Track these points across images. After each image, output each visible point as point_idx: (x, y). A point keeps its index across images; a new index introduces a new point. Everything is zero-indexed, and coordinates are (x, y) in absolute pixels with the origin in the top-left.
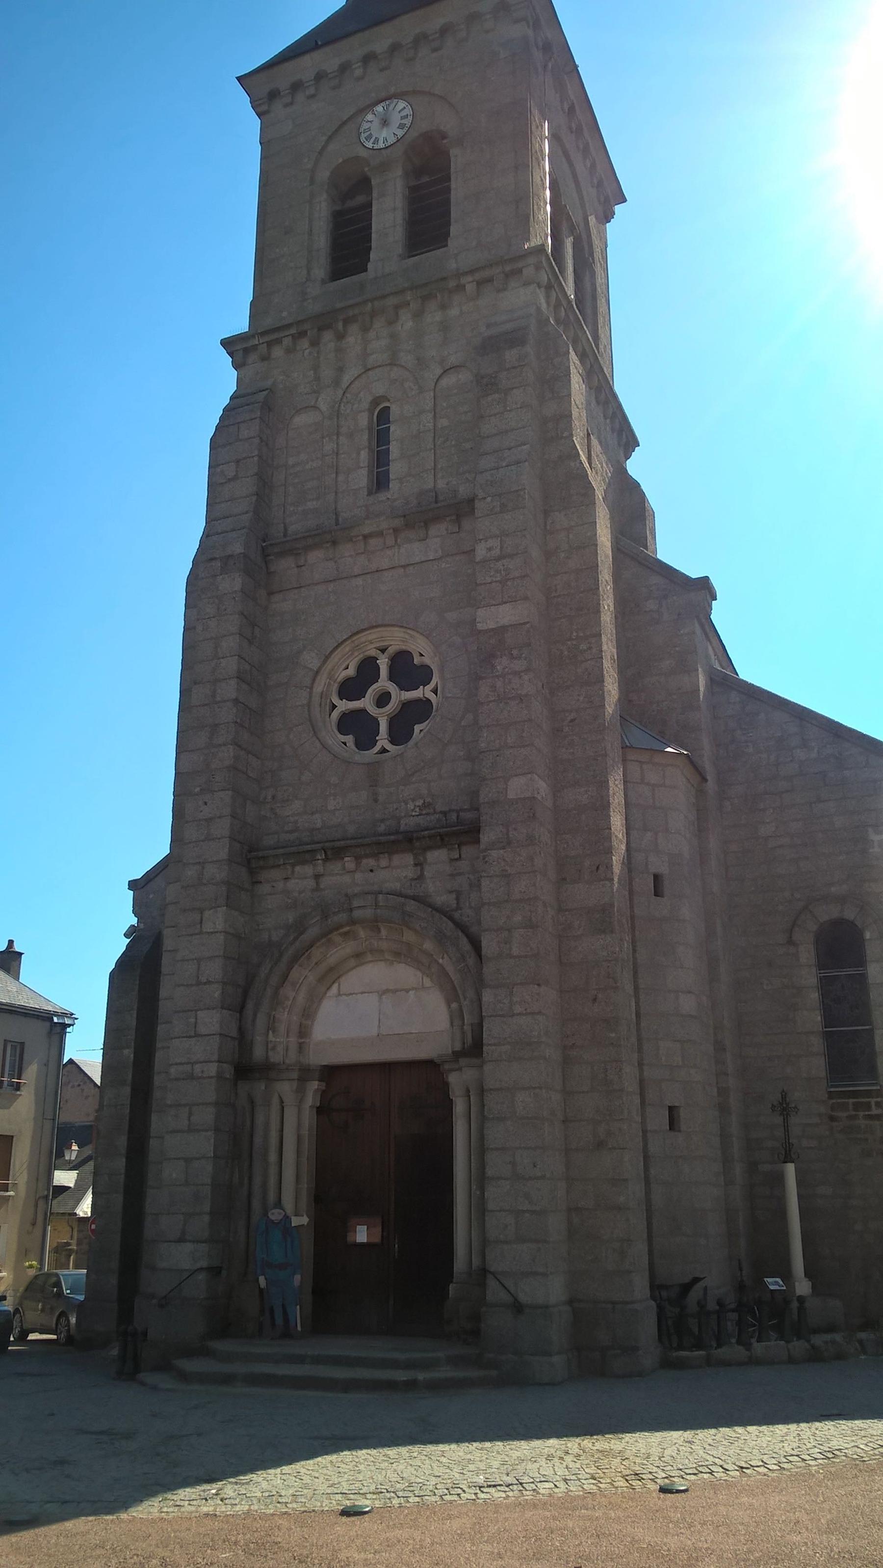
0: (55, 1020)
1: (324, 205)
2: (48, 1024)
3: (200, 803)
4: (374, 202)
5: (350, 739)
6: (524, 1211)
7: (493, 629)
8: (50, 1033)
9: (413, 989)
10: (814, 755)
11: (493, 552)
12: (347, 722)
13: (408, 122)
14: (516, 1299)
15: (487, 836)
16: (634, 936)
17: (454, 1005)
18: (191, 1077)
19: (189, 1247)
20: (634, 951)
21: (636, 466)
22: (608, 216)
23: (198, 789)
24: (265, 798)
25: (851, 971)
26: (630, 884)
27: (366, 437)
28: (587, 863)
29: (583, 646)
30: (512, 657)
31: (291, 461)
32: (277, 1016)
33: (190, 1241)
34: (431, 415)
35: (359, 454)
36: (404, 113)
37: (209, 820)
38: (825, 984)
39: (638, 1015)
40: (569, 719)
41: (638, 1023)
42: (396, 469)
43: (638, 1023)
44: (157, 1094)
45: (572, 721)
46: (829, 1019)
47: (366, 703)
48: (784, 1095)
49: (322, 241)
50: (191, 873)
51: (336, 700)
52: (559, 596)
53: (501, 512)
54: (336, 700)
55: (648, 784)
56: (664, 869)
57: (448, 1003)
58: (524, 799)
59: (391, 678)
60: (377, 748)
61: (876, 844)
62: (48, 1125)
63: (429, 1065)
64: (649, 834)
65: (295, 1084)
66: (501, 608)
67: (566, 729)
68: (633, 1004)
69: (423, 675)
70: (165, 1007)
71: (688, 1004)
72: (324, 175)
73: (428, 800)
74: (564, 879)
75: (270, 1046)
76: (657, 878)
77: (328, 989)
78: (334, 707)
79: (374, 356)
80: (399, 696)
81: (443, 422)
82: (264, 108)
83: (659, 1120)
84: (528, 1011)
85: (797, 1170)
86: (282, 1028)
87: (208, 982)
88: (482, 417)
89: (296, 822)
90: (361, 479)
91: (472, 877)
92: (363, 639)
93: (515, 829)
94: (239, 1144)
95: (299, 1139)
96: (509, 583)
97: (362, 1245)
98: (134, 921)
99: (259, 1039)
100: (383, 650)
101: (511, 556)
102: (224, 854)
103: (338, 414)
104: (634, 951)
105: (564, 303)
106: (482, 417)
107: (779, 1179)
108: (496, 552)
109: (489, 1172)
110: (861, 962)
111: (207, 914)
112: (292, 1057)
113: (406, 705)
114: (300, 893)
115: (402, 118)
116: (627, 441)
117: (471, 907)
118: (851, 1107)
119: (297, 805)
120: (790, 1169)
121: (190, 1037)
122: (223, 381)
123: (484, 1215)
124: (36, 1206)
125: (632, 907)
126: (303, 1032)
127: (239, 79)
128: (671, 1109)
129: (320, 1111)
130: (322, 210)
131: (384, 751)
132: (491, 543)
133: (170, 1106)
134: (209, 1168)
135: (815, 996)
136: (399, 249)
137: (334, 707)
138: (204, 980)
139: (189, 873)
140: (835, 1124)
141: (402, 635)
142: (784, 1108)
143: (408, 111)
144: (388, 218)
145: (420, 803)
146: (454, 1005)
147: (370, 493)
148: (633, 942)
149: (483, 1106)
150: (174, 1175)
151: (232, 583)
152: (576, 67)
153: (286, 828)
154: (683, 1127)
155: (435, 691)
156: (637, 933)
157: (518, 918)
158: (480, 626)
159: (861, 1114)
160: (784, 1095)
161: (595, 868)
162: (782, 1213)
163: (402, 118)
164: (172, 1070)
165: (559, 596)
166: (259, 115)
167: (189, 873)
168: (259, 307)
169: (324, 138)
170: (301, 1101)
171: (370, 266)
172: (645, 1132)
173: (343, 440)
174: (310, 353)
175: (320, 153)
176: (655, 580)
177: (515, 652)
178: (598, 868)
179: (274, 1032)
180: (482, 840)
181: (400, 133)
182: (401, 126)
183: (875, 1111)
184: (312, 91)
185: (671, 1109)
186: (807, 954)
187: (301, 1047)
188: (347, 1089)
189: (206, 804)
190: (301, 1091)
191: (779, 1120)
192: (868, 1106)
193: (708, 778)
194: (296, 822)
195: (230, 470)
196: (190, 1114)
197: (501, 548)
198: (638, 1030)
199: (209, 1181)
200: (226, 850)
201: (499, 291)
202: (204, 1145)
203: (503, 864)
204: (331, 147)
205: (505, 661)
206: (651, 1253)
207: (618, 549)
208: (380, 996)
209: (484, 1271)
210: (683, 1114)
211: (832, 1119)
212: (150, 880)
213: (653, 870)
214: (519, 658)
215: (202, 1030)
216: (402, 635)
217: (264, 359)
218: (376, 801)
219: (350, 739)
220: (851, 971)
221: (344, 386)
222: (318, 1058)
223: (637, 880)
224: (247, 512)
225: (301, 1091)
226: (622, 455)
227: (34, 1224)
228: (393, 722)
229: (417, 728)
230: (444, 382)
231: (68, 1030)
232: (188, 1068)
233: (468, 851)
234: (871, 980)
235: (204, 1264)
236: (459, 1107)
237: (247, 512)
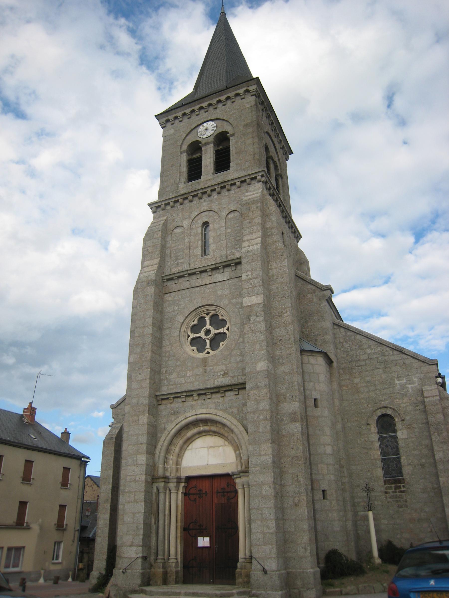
0: (83, 459)
1: (185, 157)
2: (79, 461)
3: (138, 374)
4: (203, 156)
5: (195, 348)
6: (267, 533)
7: (249, 306)
8: (81, 465)
9: (221, 446)
10: (373, 351)
11: (249, 277)
12: (194, 342)
13: (215, 129)
14: (264, 568)
15: (248, 386)
16: (307, 423)
17: (238, 452)
18: (135, 481)
19: (134, 548)
20: (308, 429)
21: (301, 245)
22: (287, 159)
23: (137, 368)
24: (163, 372)
25: (391, 434)
26: (305, 403)
27: (200, 236)
28: (288, 395)
29: (284, 311)
30: (257, 316)
31: (173, 245)
32: (168, 457)
33: (135, 546)
34: (224, 228)
35: (198, 242)
36: (213, 126)
37: (141, 380)
38: (381, 439)
39: (310, 454)
40: (280, 339)
41: (310, 458)
42: (212, 247)
43: (310, 458)
44: (121, 488)
45: (281, 340)
46: (384, 453)
47: (202, 334)
48: (367, 484)
49: (184, 169)
50: (135, 401)
51: (190, 333)
52: (274, 293)
53: (251, 262)
54: (190, 333)
55: (311, 364)
56: (318, 397)
57: (235, 451)
58: (263, 370)
59: (211, 325)
60: (206, 352)
61: (398, 384)
62: (80, 501)
63: (227, 476)
64: (312, 383)
65: (175, 484)
66: (253, 297)
67: (279, 343)
68: (308, 450)
69: (223, 323)
70: (124, 454)
71: (329, 450)
72: (185, 147)
73: (226, 372)
74: (279, 401)
75: (165, 469)
76: (315, 400)
77: (188, 446)
78: (189, 336)
79: (203, 208)
80: (214, 331)
81: (229, 231)
82: (164, 125)
83: (319, 495)
84: (267, 453)
85: (374, 514)
86: (170, 462)
87: (141, 444)
88: (243, 228)
89: (175, 381)
90: (199, 251)
91: (243, 401)
92: (200, 311)
93: (260, 382)
94: (153, 509)
95: (177, 506)
96: (255, 288)
97: (203, 535)
98: (112, 420)
99: (161, 466)
100: (207, 314)
101: (256, 278)
102: (147, 394)
103: (190, 228)
104: (308, 429)
105: (272, 188)
106: (243, 228)
107: (366, 518)
108: (250, 277)
109: (252, 518)
110: (395, 431)
111: (141, 417)
112: (173, 475)
113: (216, 335)
114: (177, 408)
115: (213, 127)
116: (298, 236)
117: (243, 413)
118: (393, 488)
119: (175, 375)
120: (370, 514)
121: (135, 465)
122: (147, 217)
123: (251, 535)
124: (74, 534)
125: (306, 412)
126: (178, 463)
127: (155, 116)
128: (324, 491)
129: (185, 494)
130: (184, 158)
131: (208, 353)
132: (248, 273)
133: (127, 492)
134: (142, 517)
135: (377, 445)
136: (212, 171)
137: (189, 336)
138: (139, 443)
139: (134, 401)
140: (387, 495)
141: (215, 308)
142: (368, 489)
143: (215, 125)
144: (208, 159)
145: (222, 373)
146: (238, 452)
147: (202, 256)
148: (307, 425)
149: (250, 491)
150: (129, 520)
151: (151, 290)
152: (273, 110)
153: (171, 383)
154: (328, 498)
155: (228, 329)
156: (309, 422)
157: (262, 417)
158: (244, 305)
159: (397, 490)
160: (367, 484)
161: (291, 397)
162: (369, 532)
163: (213, 127)
164: (128, 478)
165: (274, 293)
166: (162, 128)
167: (134, 401)
168: (161, 193)
169: (185, 135)
170: (178, 490)
171: (202, 177)
172: (313, 501)
173: (192, 237)
174: (180, 207)
175: (184, 140)
176: (310, 286)
177: (258, 314)
178: (292, 396)
179: (167, 463)
180: (247, 387)
181: (212, 132)
182: (212, 130)
183: (403, 489)
184: (181, 119)
185: (324, 491)
186: (374, 428)
187: (177, 470)
188: (196, 486)
189: (140, 374)
190: (177, 487)
191: (365, 494)
192: (400, 487)
193: (333, 360)
194: (175, 381)
195: (150, 249)
196: (135, 495)
197: (252, 275)
198: (310, 461)
199: (142, 522)
200: (148, 392)
201: (248, 184)
202: (141, 507)
203: (255, 396)
204: (188, 137)
205: (254, 317)
206: (317, 549)
207: (296, 275)
208: (208, 449)
209: (251, 557)
210: (328, 493)
211: (386, 493)
212: (119, 404)
213: (314, 397)
214: (260, 316)
215: (139, 462)
216: (215, 308)
217: (163, 209)
218: (205, 372)
219: (195, 348)
220: (391, 434)
221: (193, 218)
222: (184, 474)
223: (308, 401)
224: (156, 264)
225: (177, 487)
226: (296, 241)
227: (73, 541)
228: (212, 340)
229: (221, 344)
230: (229, 216)
231: (87, 463)
232: (133, 477)
233: (241, 392)
234: (398, 437)
235: (141, 555)
236: (240, 491)
237: (156, 264)
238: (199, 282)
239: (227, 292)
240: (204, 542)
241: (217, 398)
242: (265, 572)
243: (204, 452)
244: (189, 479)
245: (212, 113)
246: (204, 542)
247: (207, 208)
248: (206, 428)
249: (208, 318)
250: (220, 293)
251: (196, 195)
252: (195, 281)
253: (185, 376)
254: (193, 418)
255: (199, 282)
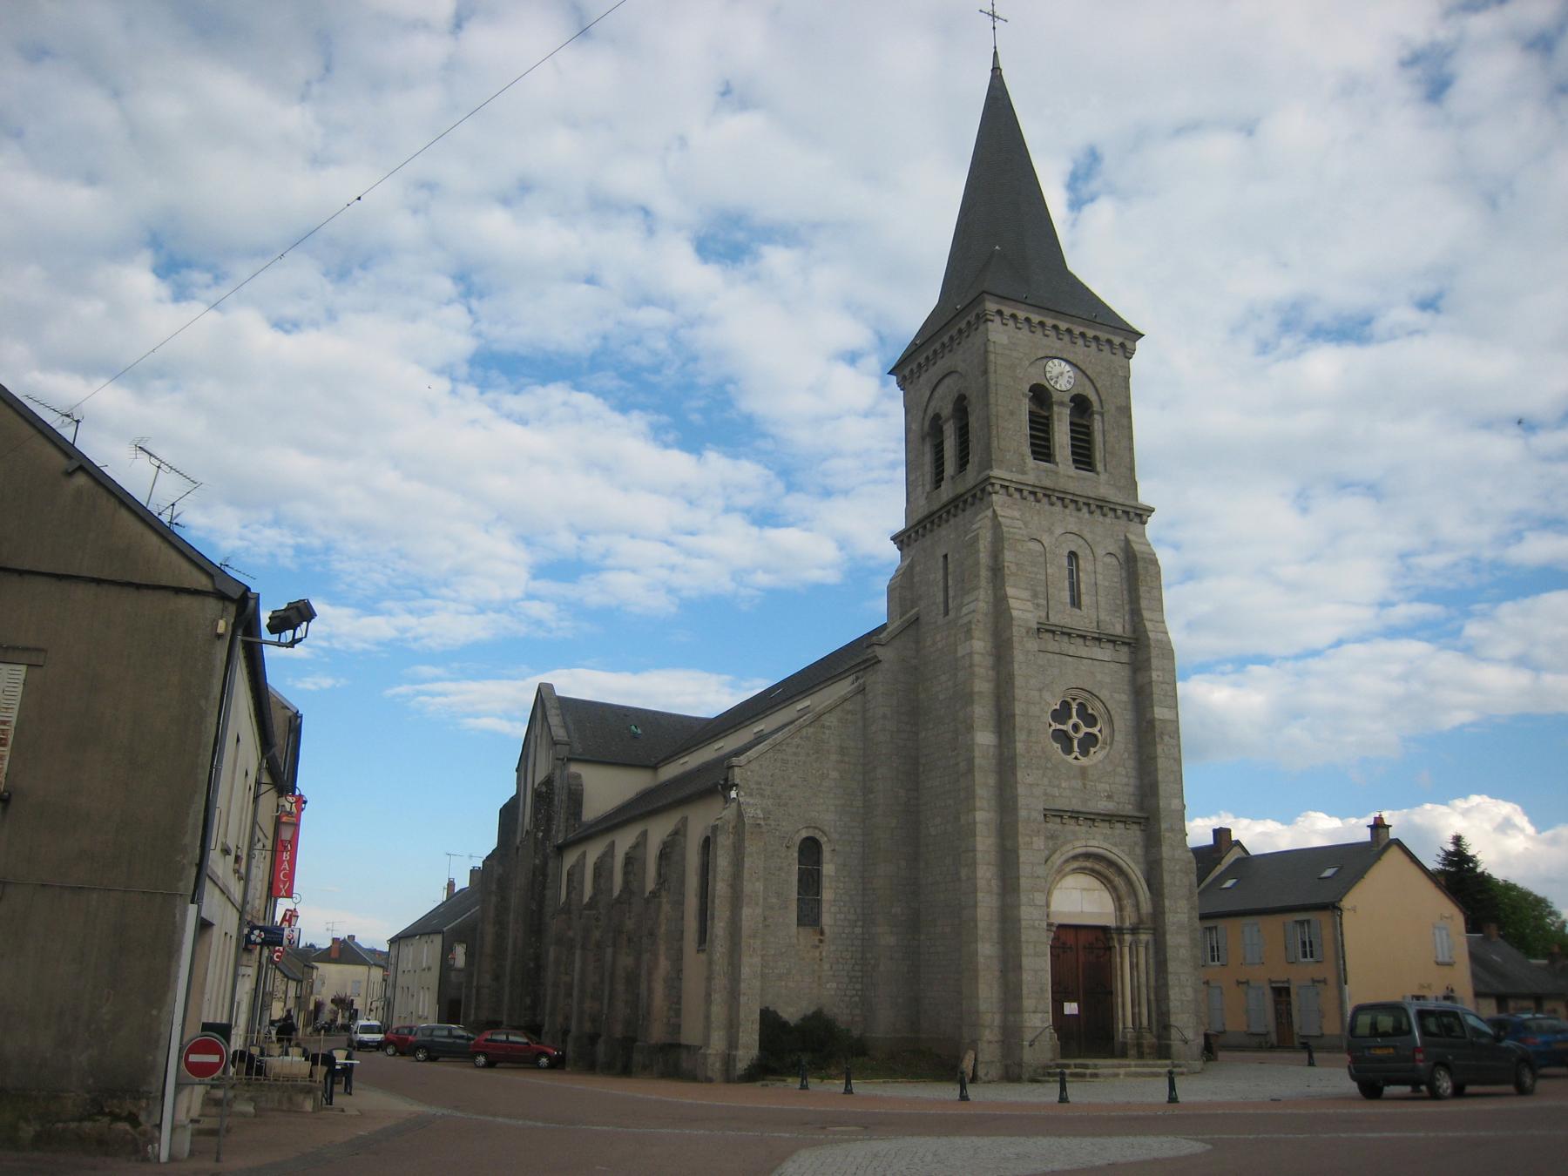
18: (1034, 928)
228: (1081, 742)
238: (1072, 650)
239: (1108, 680)
240: (1071, 1008)
241: (1103, 828)
242: (1186, 1042)
243: (1076, 894)
244: (1061, 927)
245: (1079, 352)
246: (1071, 1008)
247: (1075, 530)
248: (1097, 867)
249: (1074, 706)
250: (1099, 677)
251: (1062, 499)
252: (1065, 645)
253: (1059, 787)
254: (1083, 850)
255: (1083, 651)
